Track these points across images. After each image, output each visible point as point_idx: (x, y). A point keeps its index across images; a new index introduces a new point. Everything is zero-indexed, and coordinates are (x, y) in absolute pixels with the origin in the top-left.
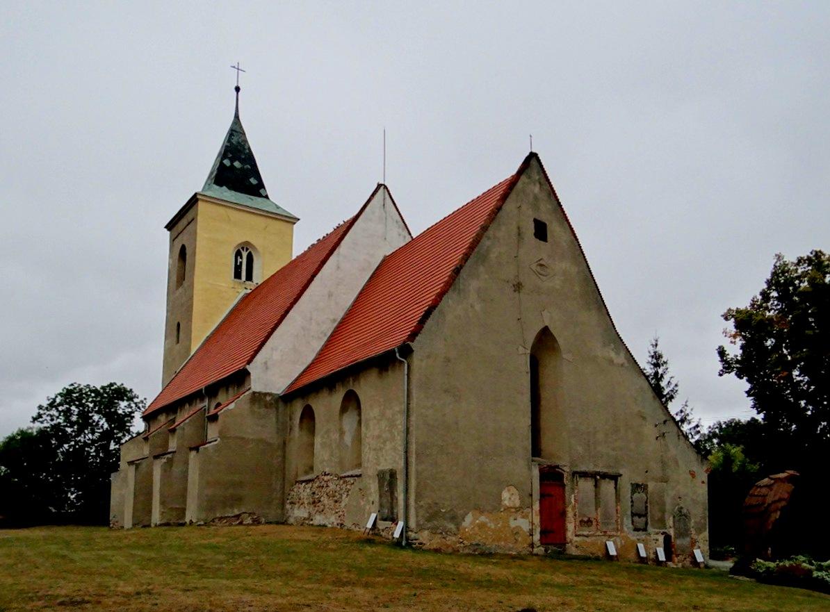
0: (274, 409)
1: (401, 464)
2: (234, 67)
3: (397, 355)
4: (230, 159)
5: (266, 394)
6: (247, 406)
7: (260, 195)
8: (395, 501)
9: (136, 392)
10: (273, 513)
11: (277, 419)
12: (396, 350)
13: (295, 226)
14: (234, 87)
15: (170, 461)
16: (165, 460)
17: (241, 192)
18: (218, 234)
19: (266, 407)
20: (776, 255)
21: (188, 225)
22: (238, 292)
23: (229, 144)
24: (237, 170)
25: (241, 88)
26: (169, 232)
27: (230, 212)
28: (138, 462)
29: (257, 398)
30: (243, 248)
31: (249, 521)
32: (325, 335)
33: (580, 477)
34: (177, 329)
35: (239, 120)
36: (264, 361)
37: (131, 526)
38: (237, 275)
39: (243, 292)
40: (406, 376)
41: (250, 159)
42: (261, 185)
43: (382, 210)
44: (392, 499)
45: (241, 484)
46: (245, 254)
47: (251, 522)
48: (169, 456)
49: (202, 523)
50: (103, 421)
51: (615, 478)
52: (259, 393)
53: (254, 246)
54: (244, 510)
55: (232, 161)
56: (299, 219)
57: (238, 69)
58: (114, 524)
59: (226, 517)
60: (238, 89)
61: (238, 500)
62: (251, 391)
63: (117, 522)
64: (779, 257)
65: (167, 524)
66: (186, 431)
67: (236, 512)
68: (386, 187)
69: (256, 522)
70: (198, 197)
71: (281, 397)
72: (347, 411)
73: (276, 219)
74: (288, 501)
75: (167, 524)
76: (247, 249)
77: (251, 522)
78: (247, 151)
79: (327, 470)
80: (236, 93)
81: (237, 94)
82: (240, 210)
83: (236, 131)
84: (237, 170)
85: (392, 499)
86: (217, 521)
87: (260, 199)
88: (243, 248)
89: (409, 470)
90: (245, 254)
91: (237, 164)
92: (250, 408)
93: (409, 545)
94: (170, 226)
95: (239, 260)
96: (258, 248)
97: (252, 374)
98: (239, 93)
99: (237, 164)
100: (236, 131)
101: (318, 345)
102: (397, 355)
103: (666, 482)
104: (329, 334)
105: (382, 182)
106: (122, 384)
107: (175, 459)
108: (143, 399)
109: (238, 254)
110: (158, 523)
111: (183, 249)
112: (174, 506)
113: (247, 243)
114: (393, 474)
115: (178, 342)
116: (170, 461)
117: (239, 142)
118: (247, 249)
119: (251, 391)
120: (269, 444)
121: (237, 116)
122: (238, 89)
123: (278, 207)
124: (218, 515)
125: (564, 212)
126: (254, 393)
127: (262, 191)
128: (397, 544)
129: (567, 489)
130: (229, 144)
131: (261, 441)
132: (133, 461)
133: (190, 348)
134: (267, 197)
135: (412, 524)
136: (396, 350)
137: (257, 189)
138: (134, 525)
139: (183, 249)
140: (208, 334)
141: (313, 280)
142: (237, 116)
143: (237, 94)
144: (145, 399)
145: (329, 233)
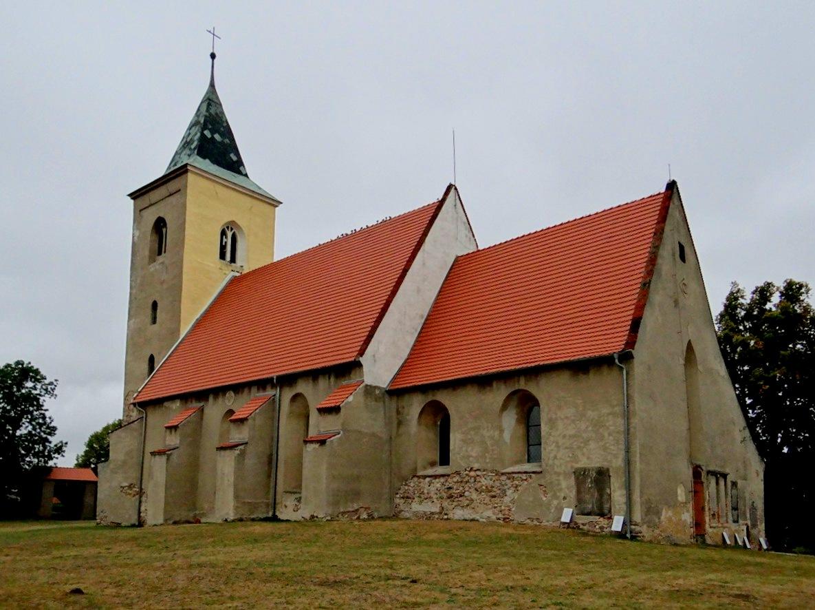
0: (382, 403)
1: (618, 463)
2: (210, 32)
3: (617, 361)
4: (210, 130)
5: (376, 387)
6: (361, 399)
7: (240, 173)
8: (606, 497)
9: (43, 372)
10: (384, 509)
11: (385, 413)
12: (616, 356)
13: (277, 208)
14: (210, 54)
15: (242, 454)
16: (237, 452)
17: (224, 168)
18: (205, 205)
19: (376, 401)
20: (732, 283)
21: (168, 196)
22: (225, 274)
23: (207, 114)
24: (213, 141)
25: (216, 53)
26: (132, 201)
27: (219, 189)
28: (169, 452)
29: (369, 390)
30: (228, 228)
31: (365, 516)
32: (416, 331)
33: (712, 475)
34: (151, 307)
35: (215, 89)
36: (373, 354)
37: (161, 521)
38: (222, 256)
39: (230, 275)
40: (625, 381)
41: (228, 133)
42: (240, 163)
43: (454, 210)
44: (601, 496)
45: (358, 478)
46: (229, 234)
47: (366, 517)
48: (242, 447)
49: (329, 518)
50: (764, 438)
51: (725, 476)
52: (370, 386)
53: (241, 228)
54: (361, 505)
55: (213, 132)
56: (281, 203)
57: (214, 35)
58: (102, 519)
59: (348, 512)
60: (213, 56)
61: (357, 495)
62: (364, 384)
63: (106, 517)
64: (734, 284)
65: (241, 520)
66: (257, 422)
67: (356, 506)
68: (456, 189)
69: (371, 517)
70: (189, 168)
71: (386, 391)
72: (506, 410)
73: (258, 199)
74: (398, 496)
75: (241, 520)
76: (232, 229)
77: (366, 517)
78: (225, 124)
79: (476, 466)
80: (211, 60)
81: (213, 61)
82: (227, 187)
83: (211, 100)
84: (213, 141)
85: (601, 496)
86: (340, 516)
87: (241, 177)
88: (228, 228)
89: (632, 469)
90: (229, 234)
91: (217, 137)
92: (365, 400)
93: (633, 538)
94: (135, 195)
95: (224, 240)
96: (244, 229)
97: (364, 367)
98: (215, 60)
99: (217, 137)
100: (211, 100)
101: (411, 340)
102: (617, 361)
103: (746, 480)
104: (419, 330)
105: (453, 183)
106: (30, 363)
107: (248, 451)
108: (53, 380)
109: (223, 233)
110: (231, 517)
111: (160, 225)
112: (247, 500)
113: (233, 222)
114: (602, 476)
115: (154, 321)
116: (242, 454)
117: (216, 114)
118: (232, 229)
119: (364, 384)
120: (380, 438)
121: (212, 85)
122: (213, 56)
123: (260, 188)
124: (342, 510)
125: (691, 236)
126: (367, 385)
127: (241, 168)
128: (620, 535)
129: (705, 485)
130: (207, 114)
131: (373, 435)
132: (165, 452)
133: (179, 331)
134: (246, 175)
135: (637, 517)
136: (616, 356)
137: (236, 166)
138: (166, 520)
139: (160, 225)
140: (198, 316)
141: (406, 274)
142: (212, 85)
143: (213, 61)
144: (56, 380)
145: (370, 225)
